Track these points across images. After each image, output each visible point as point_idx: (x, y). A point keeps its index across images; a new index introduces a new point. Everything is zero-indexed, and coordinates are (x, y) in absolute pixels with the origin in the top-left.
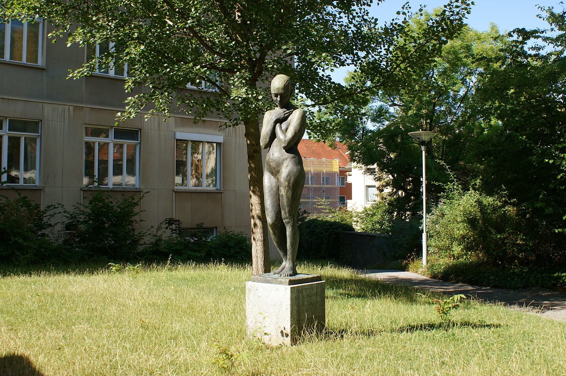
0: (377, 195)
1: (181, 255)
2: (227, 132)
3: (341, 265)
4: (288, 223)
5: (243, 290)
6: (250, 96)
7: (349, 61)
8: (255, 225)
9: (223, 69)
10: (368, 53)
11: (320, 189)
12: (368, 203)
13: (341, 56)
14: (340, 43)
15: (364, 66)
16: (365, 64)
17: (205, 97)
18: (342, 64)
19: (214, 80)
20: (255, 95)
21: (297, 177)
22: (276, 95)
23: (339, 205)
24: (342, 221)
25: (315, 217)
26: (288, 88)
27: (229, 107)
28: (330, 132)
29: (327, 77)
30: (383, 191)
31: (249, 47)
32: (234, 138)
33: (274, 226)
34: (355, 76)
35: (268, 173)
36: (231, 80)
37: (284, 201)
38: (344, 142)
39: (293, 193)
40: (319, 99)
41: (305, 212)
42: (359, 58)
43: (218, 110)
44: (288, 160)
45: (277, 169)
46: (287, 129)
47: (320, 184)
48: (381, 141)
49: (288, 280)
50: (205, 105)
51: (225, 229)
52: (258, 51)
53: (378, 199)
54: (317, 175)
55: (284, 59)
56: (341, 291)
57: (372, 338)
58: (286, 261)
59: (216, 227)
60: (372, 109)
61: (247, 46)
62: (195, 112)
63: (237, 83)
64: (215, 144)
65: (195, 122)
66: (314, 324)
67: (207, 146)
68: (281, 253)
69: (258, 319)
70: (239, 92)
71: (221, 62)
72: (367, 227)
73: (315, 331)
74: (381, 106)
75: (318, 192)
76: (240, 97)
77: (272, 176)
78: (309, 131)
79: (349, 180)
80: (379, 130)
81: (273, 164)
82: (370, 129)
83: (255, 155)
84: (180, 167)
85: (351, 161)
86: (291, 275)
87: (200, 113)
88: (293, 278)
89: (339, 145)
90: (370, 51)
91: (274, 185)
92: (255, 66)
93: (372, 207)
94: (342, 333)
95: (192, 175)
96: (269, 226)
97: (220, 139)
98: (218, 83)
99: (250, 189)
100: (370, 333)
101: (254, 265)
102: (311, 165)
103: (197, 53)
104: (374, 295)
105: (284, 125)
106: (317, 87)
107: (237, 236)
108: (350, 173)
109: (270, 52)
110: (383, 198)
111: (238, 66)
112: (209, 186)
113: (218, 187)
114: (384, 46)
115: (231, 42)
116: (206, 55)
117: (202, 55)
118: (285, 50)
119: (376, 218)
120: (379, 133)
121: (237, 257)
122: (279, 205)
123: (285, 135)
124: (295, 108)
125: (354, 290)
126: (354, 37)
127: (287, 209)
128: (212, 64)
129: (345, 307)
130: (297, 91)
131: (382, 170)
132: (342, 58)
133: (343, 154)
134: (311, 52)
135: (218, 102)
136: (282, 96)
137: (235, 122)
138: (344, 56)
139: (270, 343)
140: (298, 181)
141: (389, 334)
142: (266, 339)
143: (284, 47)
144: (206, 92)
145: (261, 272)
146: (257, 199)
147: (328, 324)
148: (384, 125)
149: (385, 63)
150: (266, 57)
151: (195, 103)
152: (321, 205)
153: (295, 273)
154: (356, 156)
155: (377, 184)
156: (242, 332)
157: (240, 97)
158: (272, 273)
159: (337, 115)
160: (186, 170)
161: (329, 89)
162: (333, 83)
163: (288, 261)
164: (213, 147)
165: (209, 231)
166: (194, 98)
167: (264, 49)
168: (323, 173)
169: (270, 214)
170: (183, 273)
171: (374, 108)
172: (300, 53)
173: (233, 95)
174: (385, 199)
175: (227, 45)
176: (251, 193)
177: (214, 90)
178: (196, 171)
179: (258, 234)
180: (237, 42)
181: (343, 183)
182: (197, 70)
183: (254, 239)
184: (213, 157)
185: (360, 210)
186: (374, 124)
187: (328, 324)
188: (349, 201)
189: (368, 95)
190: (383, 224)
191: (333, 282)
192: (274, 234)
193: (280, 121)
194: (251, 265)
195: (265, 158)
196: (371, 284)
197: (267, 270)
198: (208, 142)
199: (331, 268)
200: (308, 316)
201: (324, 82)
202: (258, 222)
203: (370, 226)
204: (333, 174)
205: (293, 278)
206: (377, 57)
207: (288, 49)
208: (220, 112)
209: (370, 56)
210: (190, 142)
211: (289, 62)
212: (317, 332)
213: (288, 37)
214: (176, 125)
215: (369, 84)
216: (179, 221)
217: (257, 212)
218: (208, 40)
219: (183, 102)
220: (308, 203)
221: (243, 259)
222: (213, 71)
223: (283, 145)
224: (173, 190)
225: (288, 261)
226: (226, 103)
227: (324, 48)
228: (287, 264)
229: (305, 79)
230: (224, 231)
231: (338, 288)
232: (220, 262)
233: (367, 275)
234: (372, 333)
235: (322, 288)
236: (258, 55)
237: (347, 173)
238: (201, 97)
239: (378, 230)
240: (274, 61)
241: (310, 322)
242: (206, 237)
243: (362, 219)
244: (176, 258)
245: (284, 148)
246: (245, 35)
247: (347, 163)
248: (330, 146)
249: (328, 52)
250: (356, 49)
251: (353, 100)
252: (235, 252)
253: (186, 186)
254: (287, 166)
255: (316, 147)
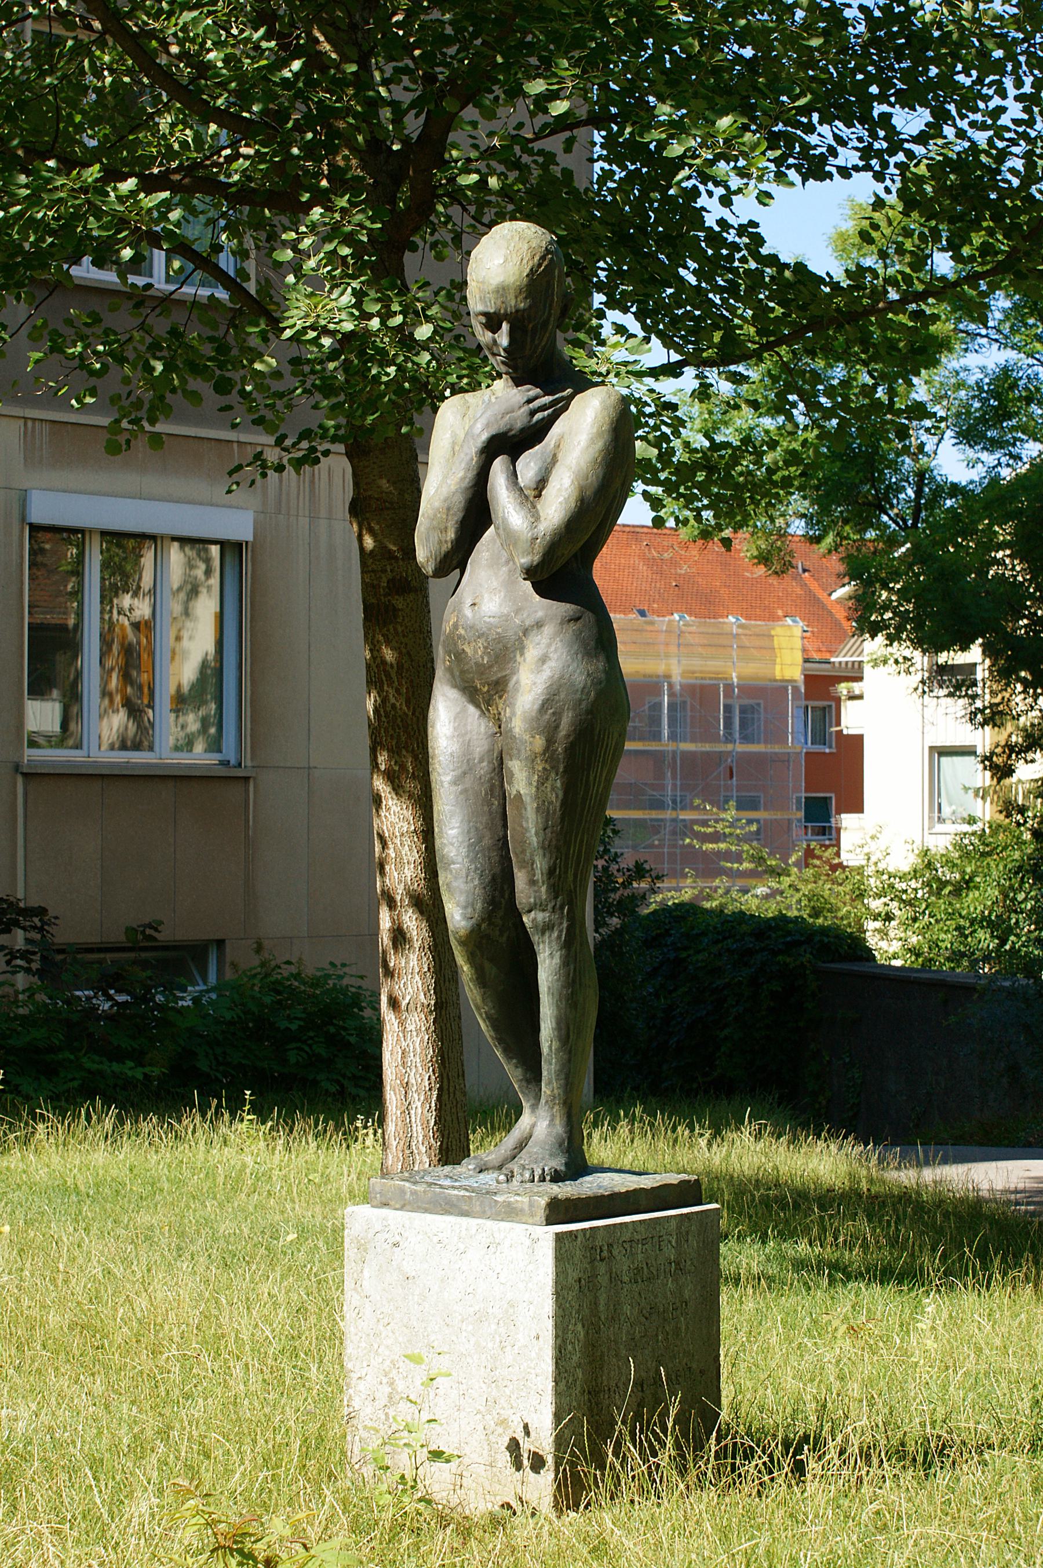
0: (982, 793)
1: (50, 1071)
2: (272, 491)
3: (805, 1126)
4: (547, 928)
5: (336, 1236)
6: (375, 323)
7: (848, 157)
8: (399, 937)
9: (241, 195)
10: (941, 116)
11: (713, 760)
12: (939, 828)
13: (810, 129)
14: (805, 66)
15: (920, 180)
16: (922, 170)
17: (161, 326)
18: (815, 169)
19: (202, 247)
20: (399, 319)
21: (589, 712)
22: (492, 322)
23: (803, 841)
24: (816, 913)
25: (687, 895)
26: (549, 285)
27: (276, 374)
28: (767, 490)
29: (742, 230)
30: (1009, 771)
31: (372, 86)
32: (304, 521)
33: (478, 941)
34: (875, 227)
35: (453, 694)
36: (285, 244)
37: (529, 826)
38: (829, 539)
39: (569, 789)
40: (700, 338)
41: (639, 871)
42: (895, 144)
43: (223, 387)
44: (548, 630)
45: (495, 675)
46: (541, 485)
47: (714, 738)
48: (1003, 533)
49: (543, 1202)
50: (159, 367)
51: (259, 949)
52: (413, 105)
53: (986, 812)
54: (700, 696)
55: (537, 146)
56: (803, 1248)
57: (942, 1478)
58: (534, 1107)
59: (220, 943)
60: (960, 385)
61: (362, 82)
62: (115, 399)
63: (312, 263)
64: (215, 550)
65: (116, 445)
66: (665, 1413)
67: (176, 556)
68: (513, 1073)
69: (401, 1386)
70: (322, 307)
71: (236, 156)
72: (935, 944)
73: (670, 1442)
74: (1006, 371)
75: (702, 777)
76: (325, 331)
77: (472, 709)
78: (657, 490)
79: (852, 719)
80: (995, 480)
81: (475, 651)
82: (953, 478)
83: (399, 602)
84: (51, 654)
85: (861, 631)
86: (557, 1177)
87: (138, 404)
88: (567, 1190)
89: (806, 556)
90: (952, 108)
91: (480, 747)
92: (397, 181)
93: (959, 846)
94: (797, 1452)
95: (105, 693)
96: (453, 943)
97: (237, 523)
98: (226, 262)
99: (375, 765)
100: (929, 1456)
101: (391, 1127)
102: (673, 649)
103: (125, 113)
104: (954, 1272)
105: (528, 465)
106: (692, 280)
107: (316, 982)
108: (856, 687)
109: (470, 112)
110: (1009, 807)
111: (318, 175)
112: (189, 744)
113: (229, 752)
114: (1019, 84)
115: (286, 63)
116: (164, 122)
117: (148, 123)
118: (543, 101)
119: (980, 901)
120: (995, 498)
121: (315, 1083)
122: (503, 844)
123: (531, 511)
124: (582, 383)
125: (865, 1246)
126: (874, 41)
127: (540, 864)
128: (196, 165)
129: (817, 1329)
130: (598, 299)
131: (1004, 674)
132: (813, 139)
133: (822, 595)
134: (664, 111)
135: (222, 348)
136: (519, 322)
137: (305, 445)
138: (825, 129)
139: (454, 1501)
140: (595, 730)
141: (1021, 1461)
142: (438, 1480)
143: (537, 87)
144: (166, 302)
145: (423, 1159)
146: (408, 814)
147: (735, 1409)
148: (1017, 458)
149: (1019, 164)
150: (452, 137)
151: (110, 353)
152: (716, 837)
153: (577, 1166)
154: (886, 607)
155: (984, 739)
156: (322, 1452)
157: (325, 331)
158: (468, 1166)
159: (790, 417)
160: (79, 675)
161: (752, 290)
162: (773, 260)
163: (543, 1111)
164: (208, 561)
165: (185, 958)
166: (107, 332)
167: (441, 95)
168: (729, 688)
169: (460, 884)
170: (56, 1159)
171: (972, 380)
172: (613, 118)
173: (295, 319)
174: (1022, 810)
175: (263, 76)
176: (380, 784)
177: (204, 292)
178: (126, 677)
179: (411, 979)
180: (315, 61)
181: (820, 736)
182: (120, 199)
183: (394, 1003)
184: (206, 607)
185: (903, 861)
186: (971, 453)
187: (735, 1409)
188: (848, 821)
189: (935, 318)
190: (1009, 931)
191: (766, 1201)
192: (481, 979)
193: (509, 444)
194: (381, 1122)
195: (441, 619)
196: (946, 1215)
197: (451, 1150)
198: (184, 541)
199: (758, 1136)
200: (637, 1373)
201: (730, 258)
202: (412, 922)
203: (947, 940)
204: (777, 690)
205: (567, 1190)
206: (981, 138)
207: (552, 96)
208: (234, 398)
209: (949, 131)
210: (96, 540)
211: (564, 160)
212: (678, 1446)
213: (555, 37)
214: (31, 459)
215: (943, 264)
216: (41, 911)
217: (409, 872)
218: (174, 49)
219: (57, 349)
220: (656, 826)
221: (342, 1092)
222: (198, 201)
223: (525, 560)
224: (17, 768)
225: (543, 1111)
226: (260, 356)
227: (728, 91)
228: (538, 1124)
229: (636, 245)
230: (256, 962)
231: (787, 1233)
232: (235, 1107)
233: (929, 1175)
234: (941, 1454)
235: (708, 1237)
236: (414, 124)
237: (843, 688)
238: (142, 327)
239: (986, 959)
240: (490, 153)
241: (648, 1399)
242: (170, 988)
243: (909, 903)
244: (27, 1088)
245: (531, 573)
246: (354, 27)
247: (841, 638)
248: (764, 559)
249: (747, 110)
250: (883, 98)
251: (865, 341)
252: (306, 1063)
253: (78, 746)
254: (543, 660)
255: (694, 560)
